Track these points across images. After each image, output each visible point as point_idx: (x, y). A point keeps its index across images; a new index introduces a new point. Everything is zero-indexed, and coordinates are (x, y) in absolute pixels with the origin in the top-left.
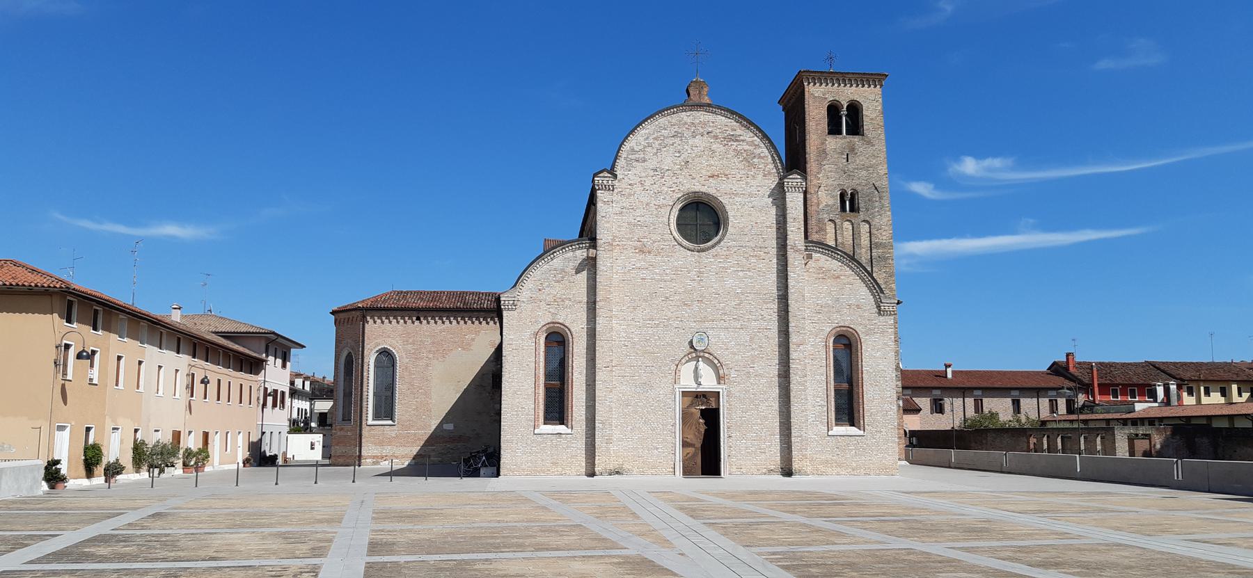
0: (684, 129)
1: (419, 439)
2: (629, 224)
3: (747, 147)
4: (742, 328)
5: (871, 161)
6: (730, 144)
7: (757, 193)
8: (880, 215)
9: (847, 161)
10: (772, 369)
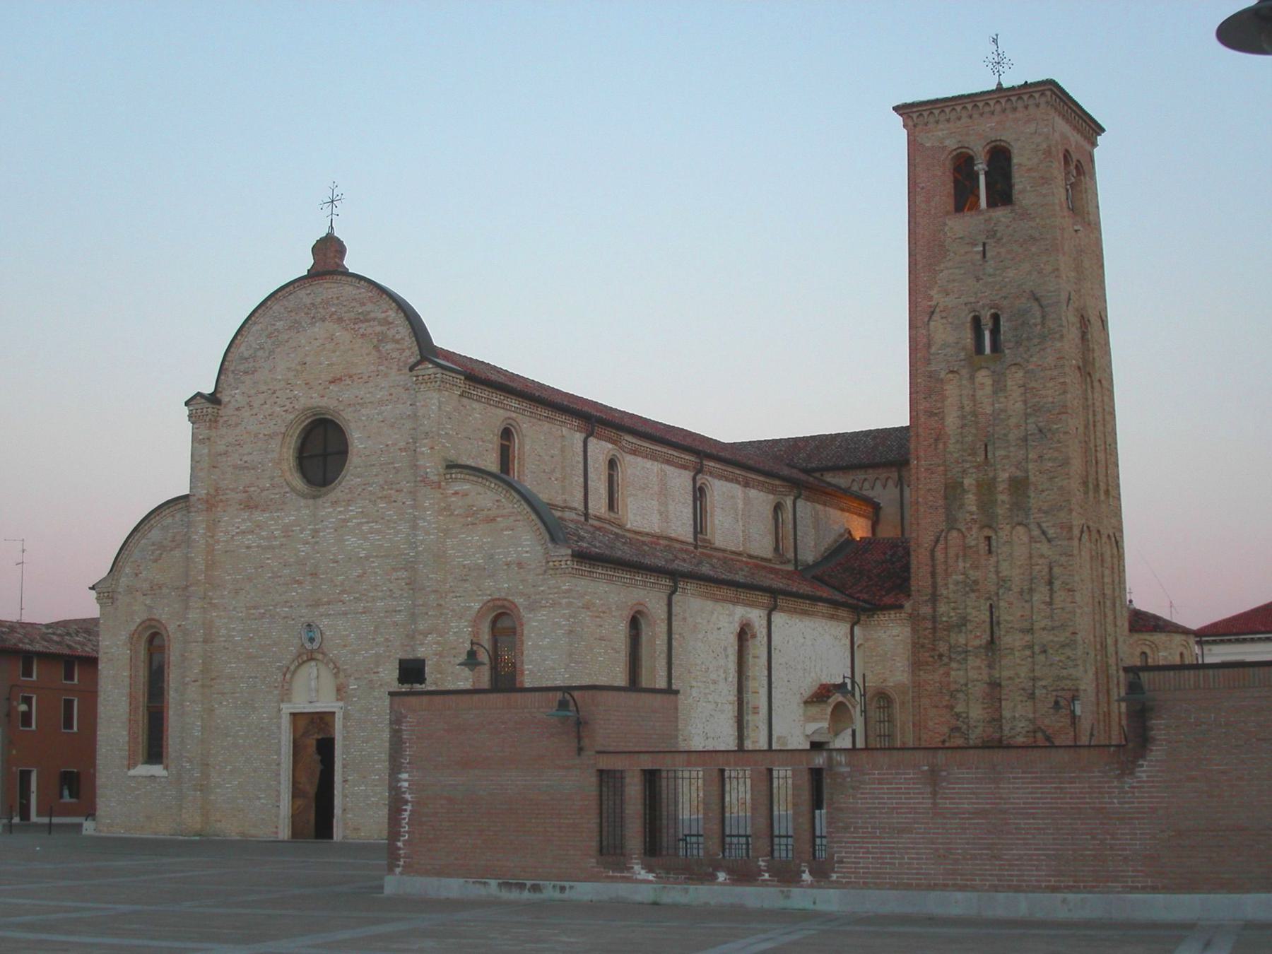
0: (303, 315)
2: (235, 467)
3: (378, 329)
4: (364, 613)
6: (357, 326)
7: (389, 398)
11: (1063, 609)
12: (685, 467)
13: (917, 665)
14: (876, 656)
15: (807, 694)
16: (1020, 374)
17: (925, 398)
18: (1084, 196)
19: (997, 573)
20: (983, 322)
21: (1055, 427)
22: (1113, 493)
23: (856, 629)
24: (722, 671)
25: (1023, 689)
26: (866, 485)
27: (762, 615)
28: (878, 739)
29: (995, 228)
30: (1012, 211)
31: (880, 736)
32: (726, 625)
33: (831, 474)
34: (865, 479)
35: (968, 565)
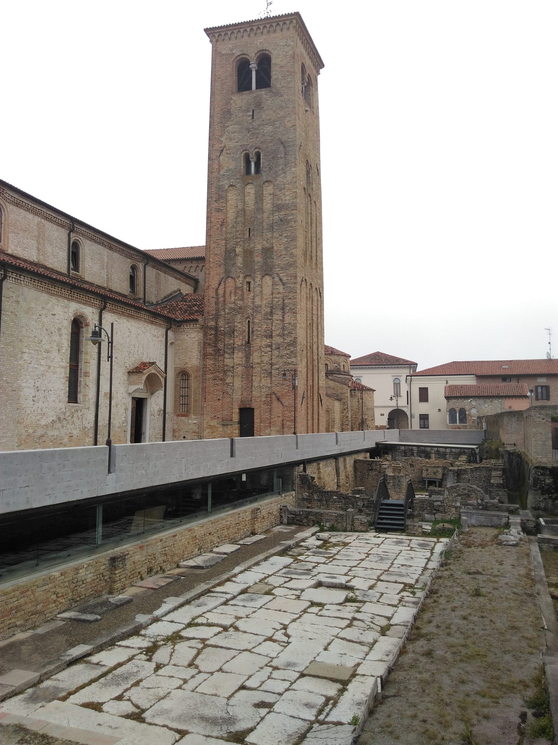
1: (105, 426)
5: (278, 114)
8: (285, 173)
9: (253, 118)
10: (321, 674)
11: (290, 324)
12: (63, 226)
13: (205, 356)
14: (182, 349)
15: (131, 368)
16: (271, 187)
17: (216, 201)
18: (311, 97)
19: (253, 303)
20: (251, 156)
21: (289, 218)
22: (319, 266)
23: (170, 333)
24: (55, 344)
25: (265, 370)
26: (192, 270)
27: (95, 312)
28: (181, 398)
29: (260, 101)
30: (270, 91)
31: (183, 396)
32: (61, 313)
33: (174, 264)
34: (191, 266)
35: (237, 298)
